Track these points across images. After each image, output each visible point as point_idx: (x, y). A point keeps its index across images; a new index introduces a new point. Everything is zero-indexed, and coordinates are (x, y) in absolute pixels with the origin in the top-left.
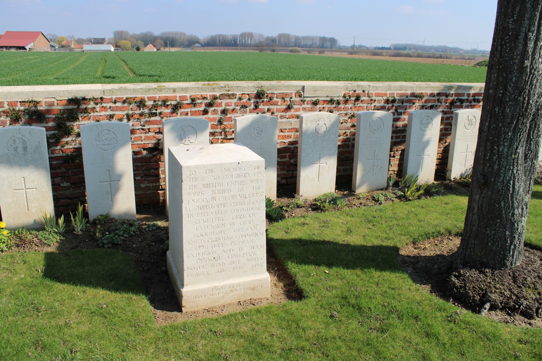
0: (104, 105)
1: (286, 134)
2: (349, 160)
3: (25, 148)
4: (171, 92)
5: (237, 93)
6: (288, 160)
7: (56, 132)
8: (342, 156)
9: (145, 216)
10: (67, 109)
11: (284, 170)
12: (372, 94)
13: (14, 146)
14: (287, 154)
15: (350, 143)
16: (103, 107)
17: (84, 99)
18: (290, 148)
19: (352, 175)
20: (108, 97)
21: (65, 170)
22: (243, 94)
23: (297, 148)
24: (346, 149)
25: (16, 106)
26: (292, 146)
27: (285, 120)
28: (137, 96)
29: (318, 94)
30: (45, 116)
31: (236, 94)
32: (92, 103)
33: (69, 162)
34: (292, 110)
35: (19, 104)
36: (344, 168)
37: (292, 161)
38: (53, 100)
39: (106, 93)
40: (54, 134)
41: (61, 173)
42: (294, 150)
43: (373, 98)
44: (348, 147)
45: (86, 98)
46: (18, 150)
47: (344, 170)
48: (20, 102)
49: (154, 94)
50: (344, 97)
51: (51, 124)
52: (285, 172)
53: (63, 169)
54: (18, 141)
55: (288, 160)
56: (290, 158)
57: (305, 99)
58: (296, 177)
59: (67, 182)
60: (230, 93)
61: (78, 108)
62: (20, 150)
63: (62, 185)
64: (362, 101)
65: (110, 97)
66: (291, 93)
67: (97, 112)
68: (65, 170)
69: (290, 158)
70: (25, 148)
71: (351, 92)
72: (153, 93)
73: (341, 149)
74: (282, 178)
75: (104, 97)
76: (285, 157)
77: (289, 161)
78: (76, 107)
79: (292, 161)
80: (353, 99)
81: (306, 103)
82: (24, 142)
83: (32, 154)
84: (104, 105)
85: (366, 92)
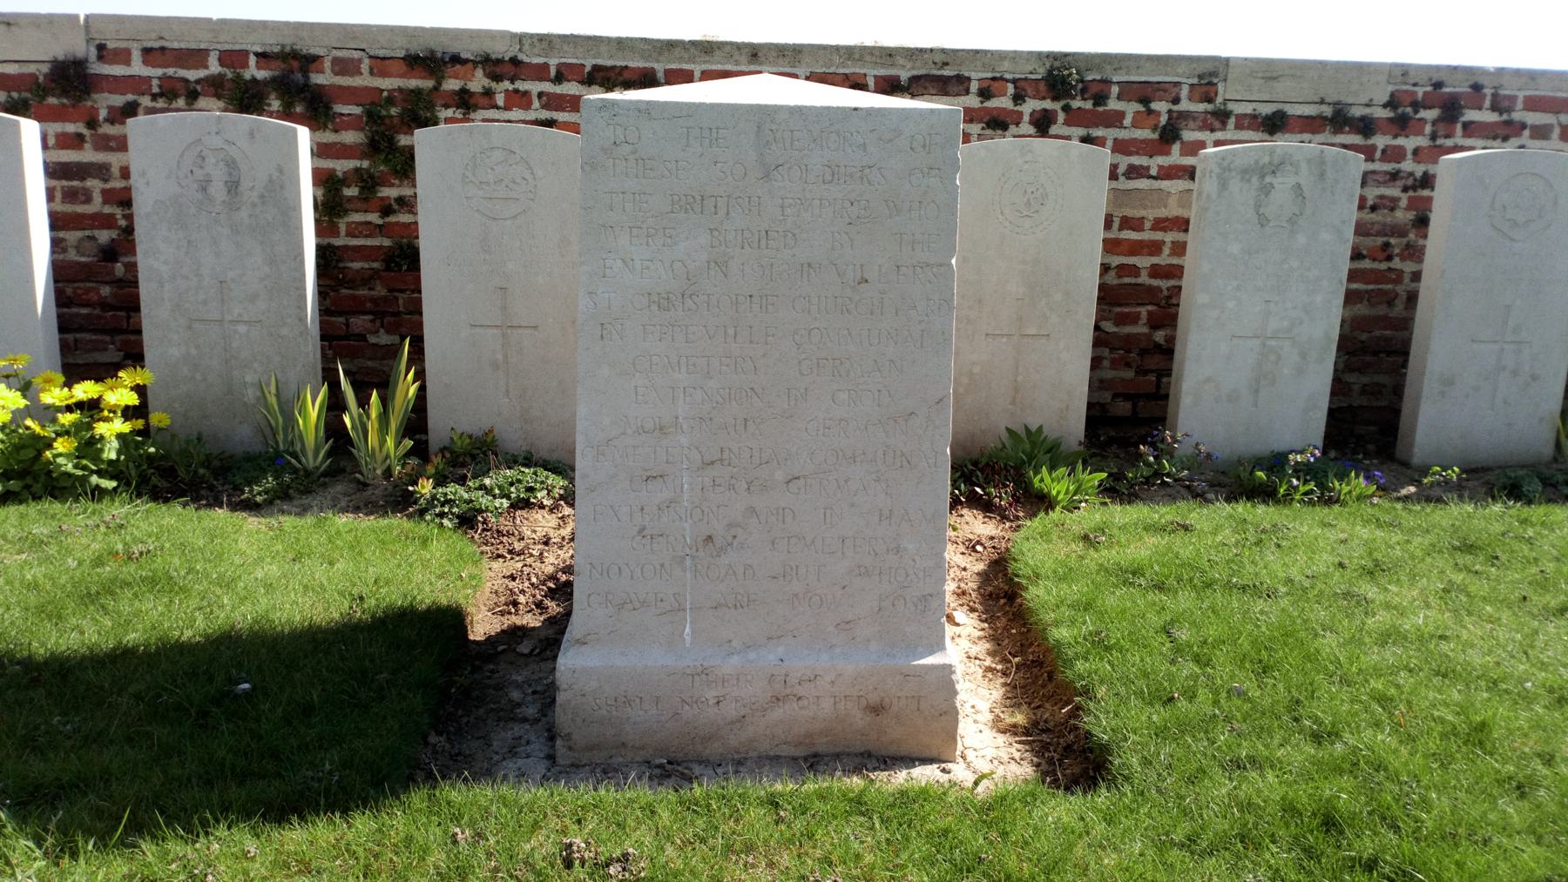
0: (522, 86)
1: (1146, 235)
2: (1389, 354)
3: (233, 186)
4: (744, 59)
5: (973, 75)
6: (1145, 330)
7: (365, 164)
8: (1364, 337)
9: (921, 662)
10: (400, 90)
11: (1128, 365)
12: (1513, 99)
13: (199, 173)
14: (1144, 311)
15: (1400, 289)
16: (516, 91)
17: (456, 59)
18: (1152, 290)
19: (1396, 412)
20: (536, 60)
21: (384, 292)
22: (994, 79)
23: (1180, 288)
24: (1381, 310)
25: (246, 65)
26: (1164, 284)
27: (1143, 184)
28: (631, 64)
29: (1283, 90)
30: (328, 108)
31: (969, 79)
32: (479, 73)
33: (399, 266)
34: (1176, 148)
35: (252, 60)
36: (1365, 380)
37: (1159, 336)
38: (356, 55)
39: (527, 47)
40: (357, 170)
41: (373, 300)
42: (1170, 297)
43: (1517, 116)
44: (1390, 303)
45: (464, 55)
46: (212, 190)
47: (1364, 390)
48: (257, 54)
49: (690, 61)
50: (1392, 103)
51: (350, 137)
52: (1129, 374)
53: (380, 291)
54: (211, 160)
55: (1145, 330)
56: (1155, 324)
57: (1230, 106)
58: (1167, 397)
59: (388, 332)
60: (947, 72)
61: (436, 89)
62: (218, 190)
63: (372, 339)
64: (1466, 125)
65: (540, 60)
66: (1177, 84)
67: (498, 108)
68: (384, 292)
69: (1155, 324)
70: (233, 186)
71: (1420, 91)
72: (681, 59)
73: (1362, 309)
74: (93, 437)
75: (522, 57)
76: (1133, 319)
77: (1148, 337)
78: (428, 84)
79: (1159, 336)
80: (1430, 114)
81: (1232, 121)
82: (231, 165)
83: (254, 205)
84: (522, 86)
85: (1488, 91)
